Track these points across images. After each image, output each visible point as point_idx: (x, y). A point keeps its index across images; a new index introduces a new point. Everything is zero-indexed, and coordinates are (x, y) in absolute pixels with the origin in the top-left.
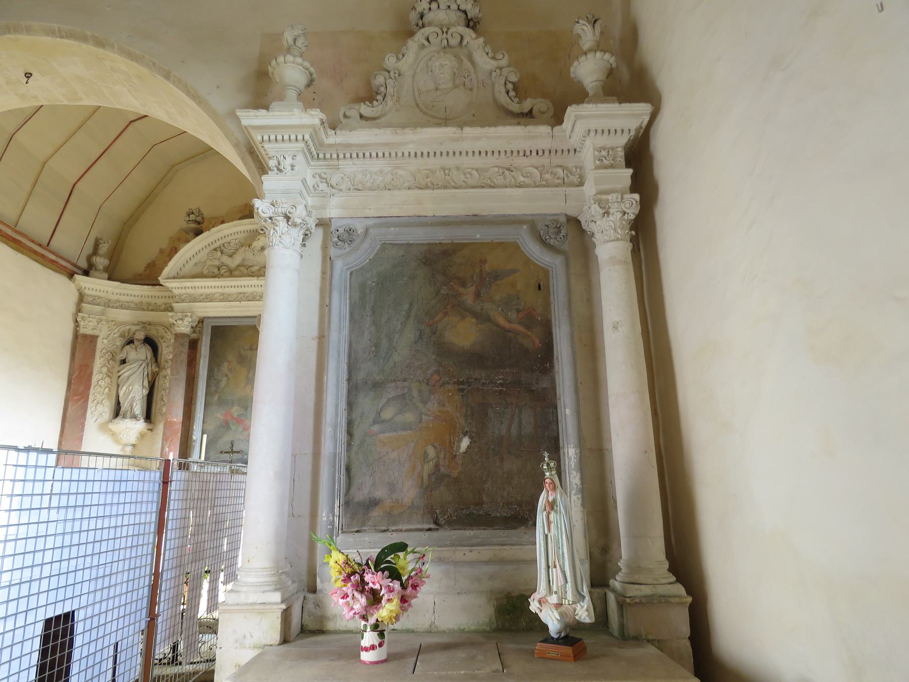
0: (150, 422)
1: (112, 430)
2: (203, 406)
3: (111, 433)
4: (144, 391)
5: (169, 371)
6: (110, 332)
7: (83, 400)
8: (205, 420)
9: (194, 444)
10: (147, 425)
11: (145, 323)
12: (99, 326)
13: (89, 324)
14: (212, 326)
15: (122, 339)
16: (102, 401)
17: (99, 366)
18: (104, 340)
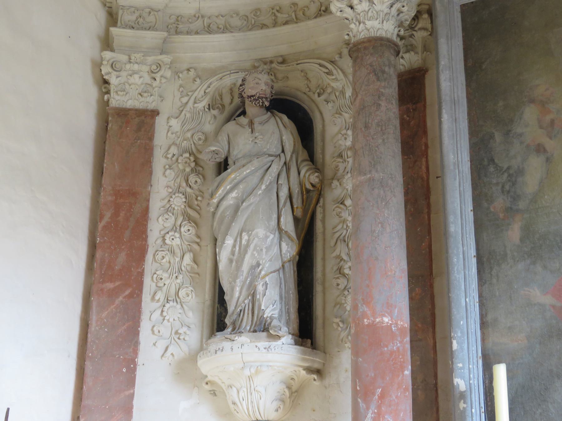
0: (314, 346)
1: (210, 378)
2: (474, 270)
3: (208, 387)
4: (284, 245)
5: (349, 183)
6: (185, 100)
7: (127, 292)
8: (489, 318)
9: (462, 405)
10: (304, 353)
11: (271, 62)
12: (155, 84)
13: (132, 80)
14: (463, 6)
15: (215, 112)
16: (177, 294)
17: (164, 193)
18: (173, 122)
